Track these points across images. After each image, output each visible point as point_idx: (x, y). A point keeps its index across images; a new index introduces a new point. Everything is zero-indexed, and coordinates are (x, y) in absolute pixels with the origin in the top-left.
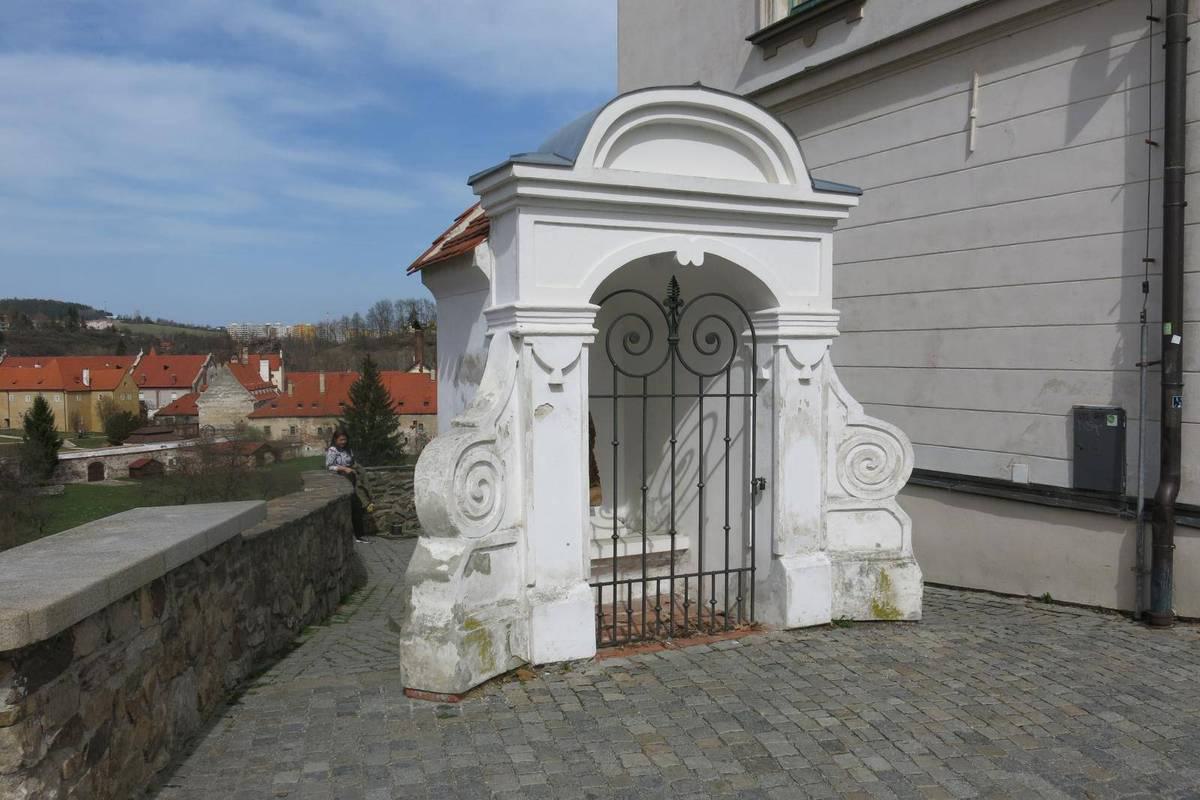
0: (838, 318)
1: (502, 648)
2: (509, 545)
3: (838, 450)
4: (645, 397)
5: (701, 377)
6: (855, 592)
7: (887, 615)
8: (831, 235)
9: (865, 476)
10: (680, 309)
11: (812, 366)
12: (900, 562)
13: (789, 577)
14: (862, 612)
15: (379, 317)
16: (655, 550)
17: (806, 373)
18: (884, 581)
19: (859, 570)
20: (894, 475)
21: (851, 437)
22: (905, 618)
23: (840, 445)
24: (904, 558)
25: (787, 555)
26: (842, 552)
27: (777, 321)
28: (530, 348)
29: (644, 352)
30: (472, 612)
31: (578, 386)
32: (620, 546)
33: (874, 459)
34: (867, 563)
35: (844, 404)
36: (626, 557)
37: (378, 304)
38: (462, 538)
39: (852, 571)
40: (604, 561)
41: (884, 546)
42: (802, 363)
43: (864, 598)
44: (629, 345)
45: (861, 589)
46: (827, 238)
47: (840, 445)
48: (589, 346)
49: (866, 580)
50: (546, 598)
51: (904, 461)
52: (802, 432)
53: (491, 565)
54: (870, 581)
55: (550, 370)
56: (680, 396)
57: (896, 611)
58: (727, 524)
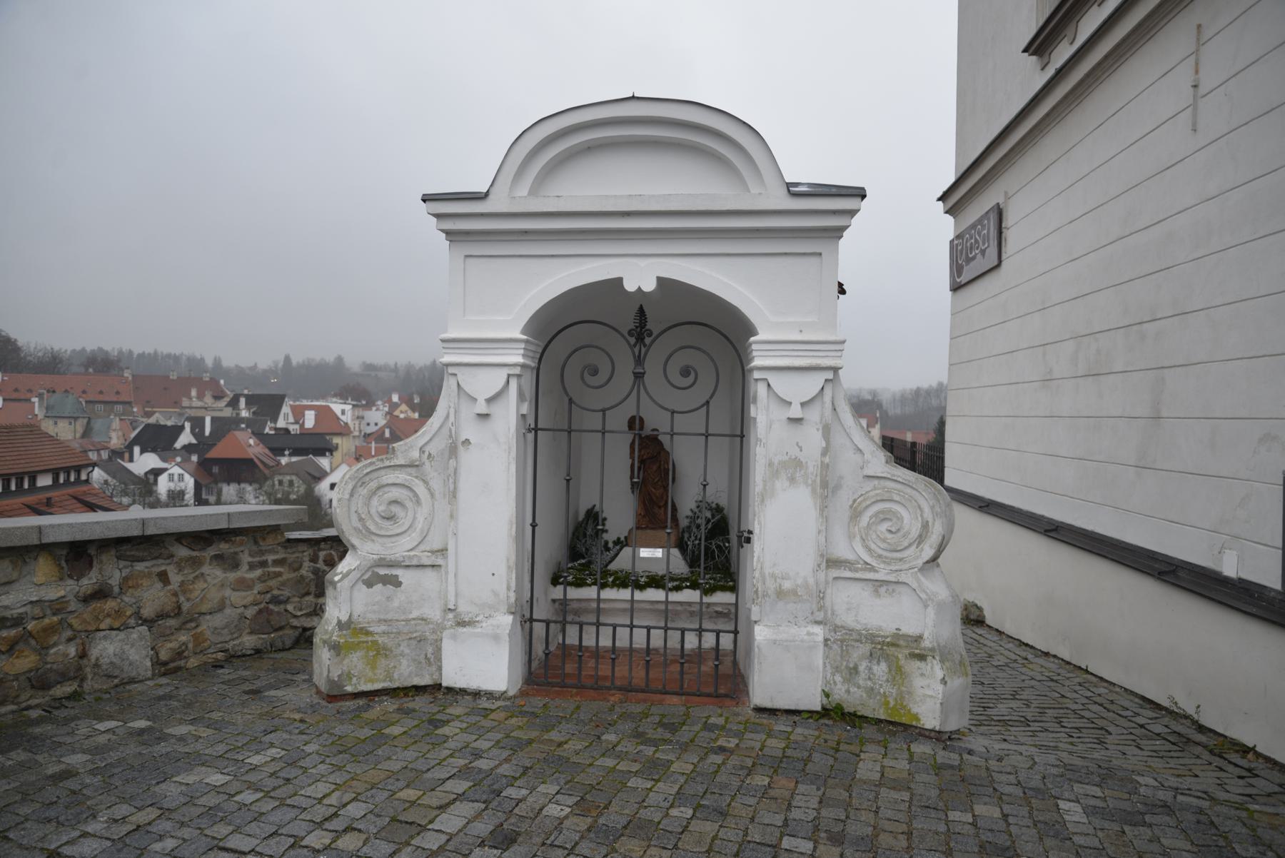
4: (707, 436)
5: (673, 412)
14: (873, 709)
17: (796, 412)
29: (589, 386)
48: (519, 376)
52: (792, 480)
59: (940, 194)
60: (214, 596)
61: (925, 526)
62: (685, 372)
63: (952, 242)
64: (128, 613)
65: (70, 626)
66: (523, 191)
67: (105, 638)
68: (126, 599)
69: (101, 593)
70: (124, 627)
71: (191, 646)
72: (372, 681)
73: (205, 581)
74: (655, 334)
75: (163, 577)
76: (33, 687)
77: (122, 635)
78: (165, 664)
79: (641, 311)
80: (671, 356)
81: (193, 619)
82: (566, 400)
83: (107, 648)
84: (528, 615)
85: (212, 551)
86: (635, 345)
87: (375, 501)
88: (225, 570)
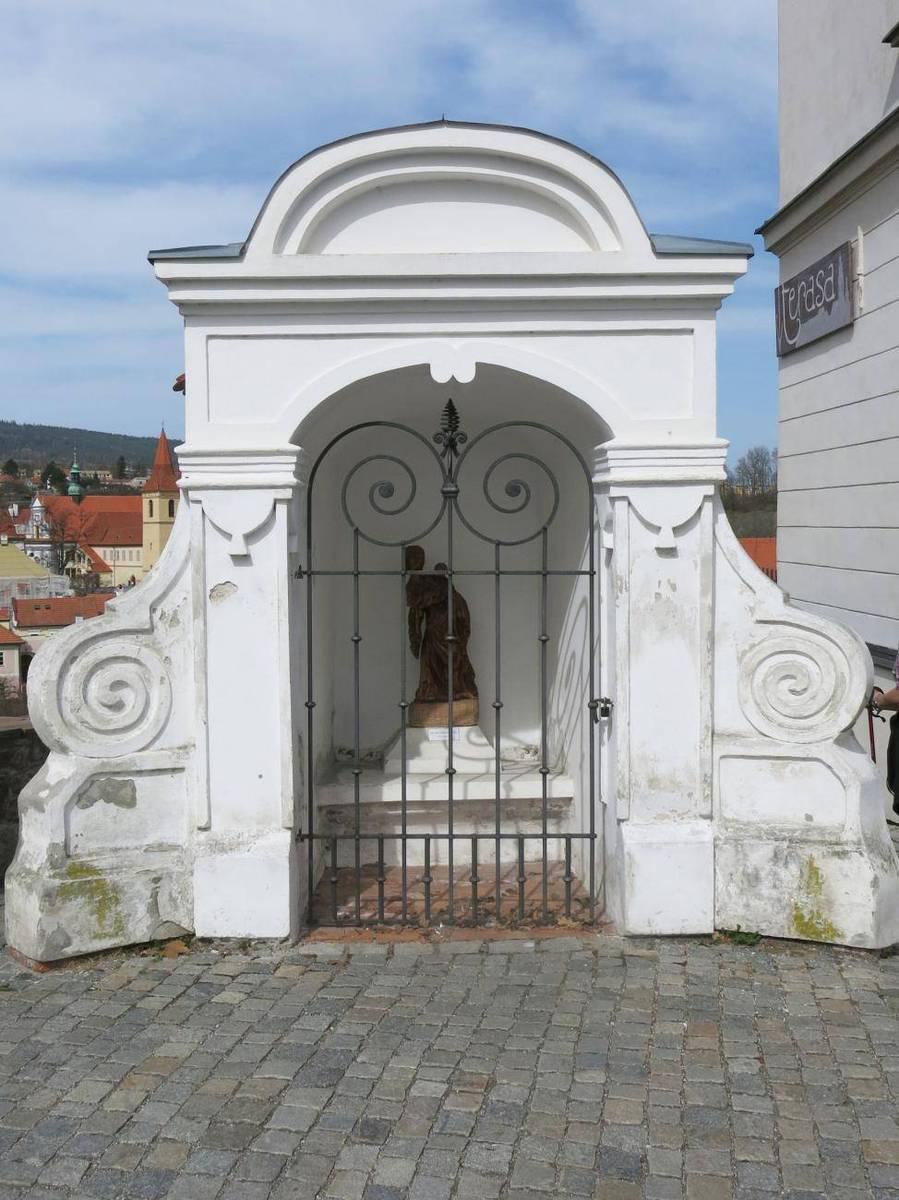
0: (724, 452)
1: (142, 910)
2: (174, 770)
3: (740, 660)
4: (545, 574)
5: (498, 544)
6: (765, 889)
7: (819, 934)
8: (712, 323)
9: (786, 705)
11: (674, 529)
12: (838, 848)
13: (629, 854)
14: (778, 924)
15: (752, 470)
16: (514, 795)
17: (667, 539)
18: (812, 877)
19: (771, 854)
20: (833, 702)
21: (763, 641)
22: (847, 942)
23: (744, 653)
24: (846, 843)
25: (635, 819)
26: (748, 823)
27: (607, 460)
28: (199, 505)
30: (90, 855)
31: (274, 554)
32: (458, 786)
33: (799, 677)
34: (785, 844)
35: (751, 588)
36: (423, 804)
37: (751, 453)
38: (73, 757)
39: (759, 855)
40: (436, 804)
41: (820, 819)
42: (659, 525)
43: (779, 900)
45: (775, 886)
46: (705, 329)
47: (744, 653)
48: (288, 501)
49: (783, 873)
50: (218, 847)
51: (851, 679)
53: (137, 795)
54: (790, 874)
55: (228, 536)
56: (365, 573)
57: (835, 933)
59: (761, 224)
61: (840, 682)
62: (513, 490)
63: (778, 291)
72: (97, 936)
74: (469, 441)
79: (451, 409)
80: (492, 467)
82: (351, 530)
84: (305, 831)
86: (443, 455)
87: (93, 686)
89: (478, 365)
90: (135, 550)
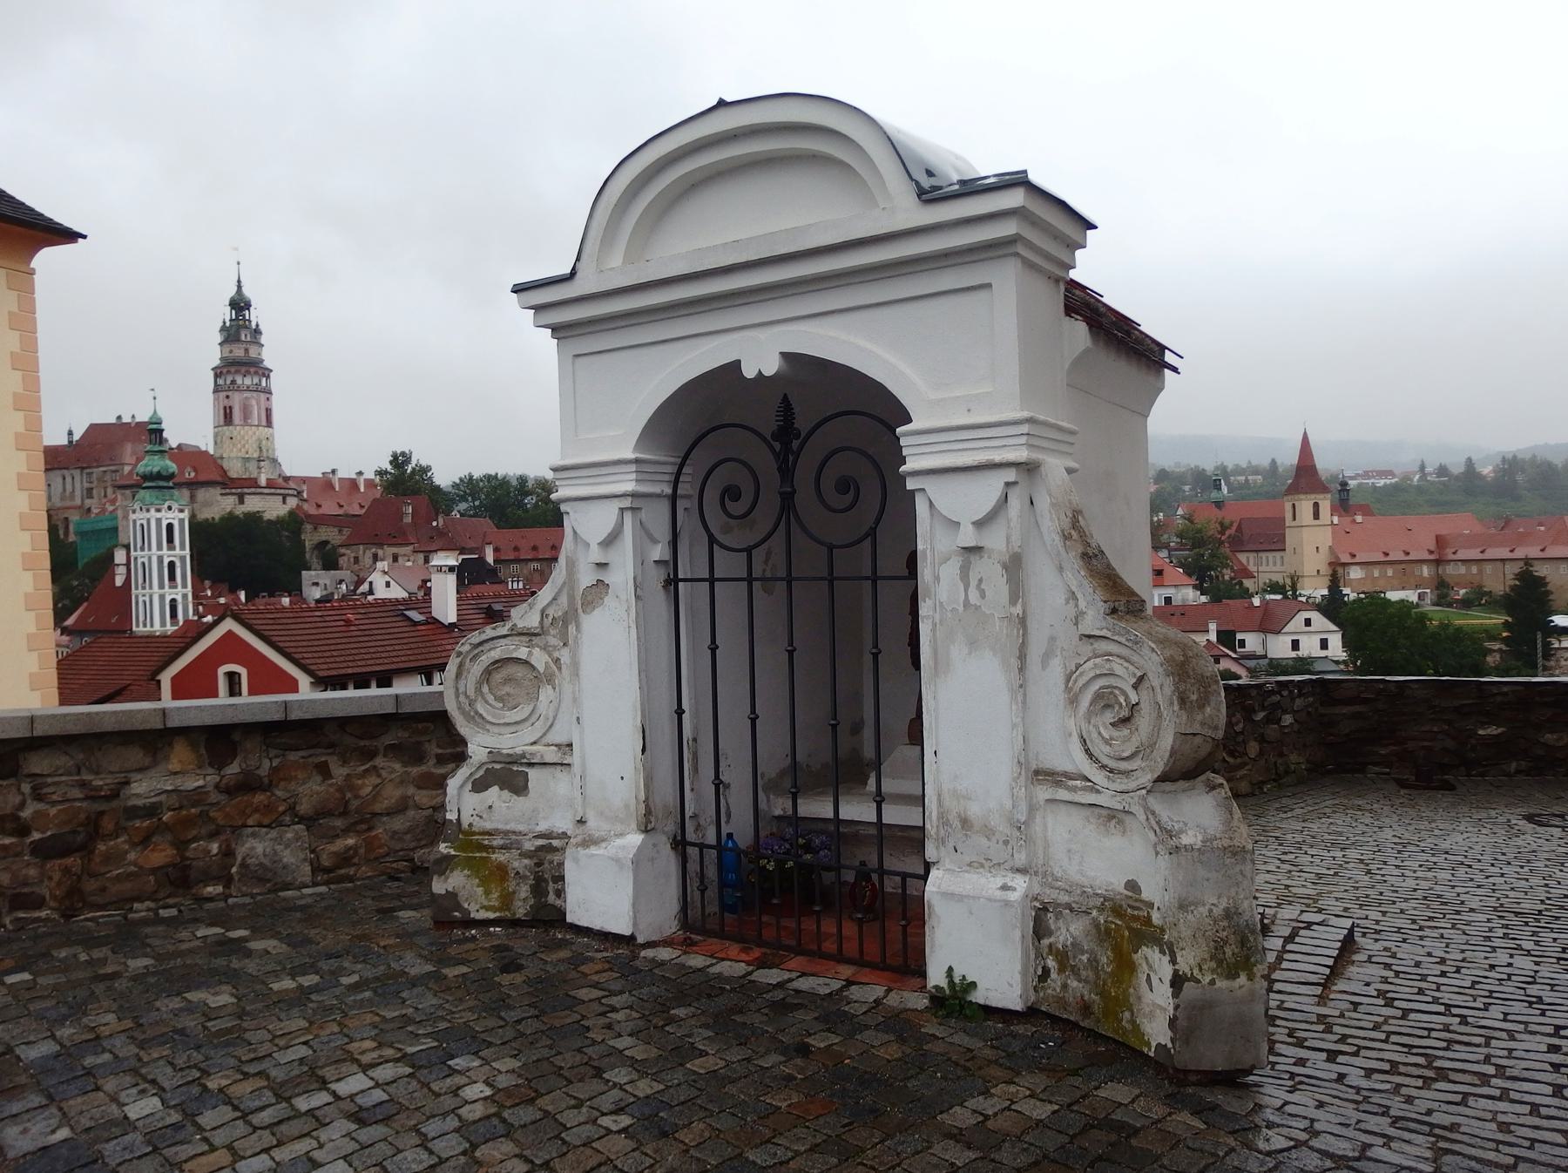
5: (831, 548)
10: (795, 444)
17: (968, 537)
44: (729, 504)
52: (973, 644)
58: (753, 710)
60: (392, 794)
64: (281, 809)
65: (212, 820)
66: (616, 259)
67: (254, 835)
68: (279, 793)
69: (247, 785)
70: (276, 823)
71: (362, 851)
73: (379, 776)
75: (324, 771)
76: (171, 883)
77: (274, 834)
78: (327, 870)
81: (364, 820)
83: (256, 847)
85: (388, 740)
88: (405, 764)
89: (785, 355)
90: (1278, 555)
